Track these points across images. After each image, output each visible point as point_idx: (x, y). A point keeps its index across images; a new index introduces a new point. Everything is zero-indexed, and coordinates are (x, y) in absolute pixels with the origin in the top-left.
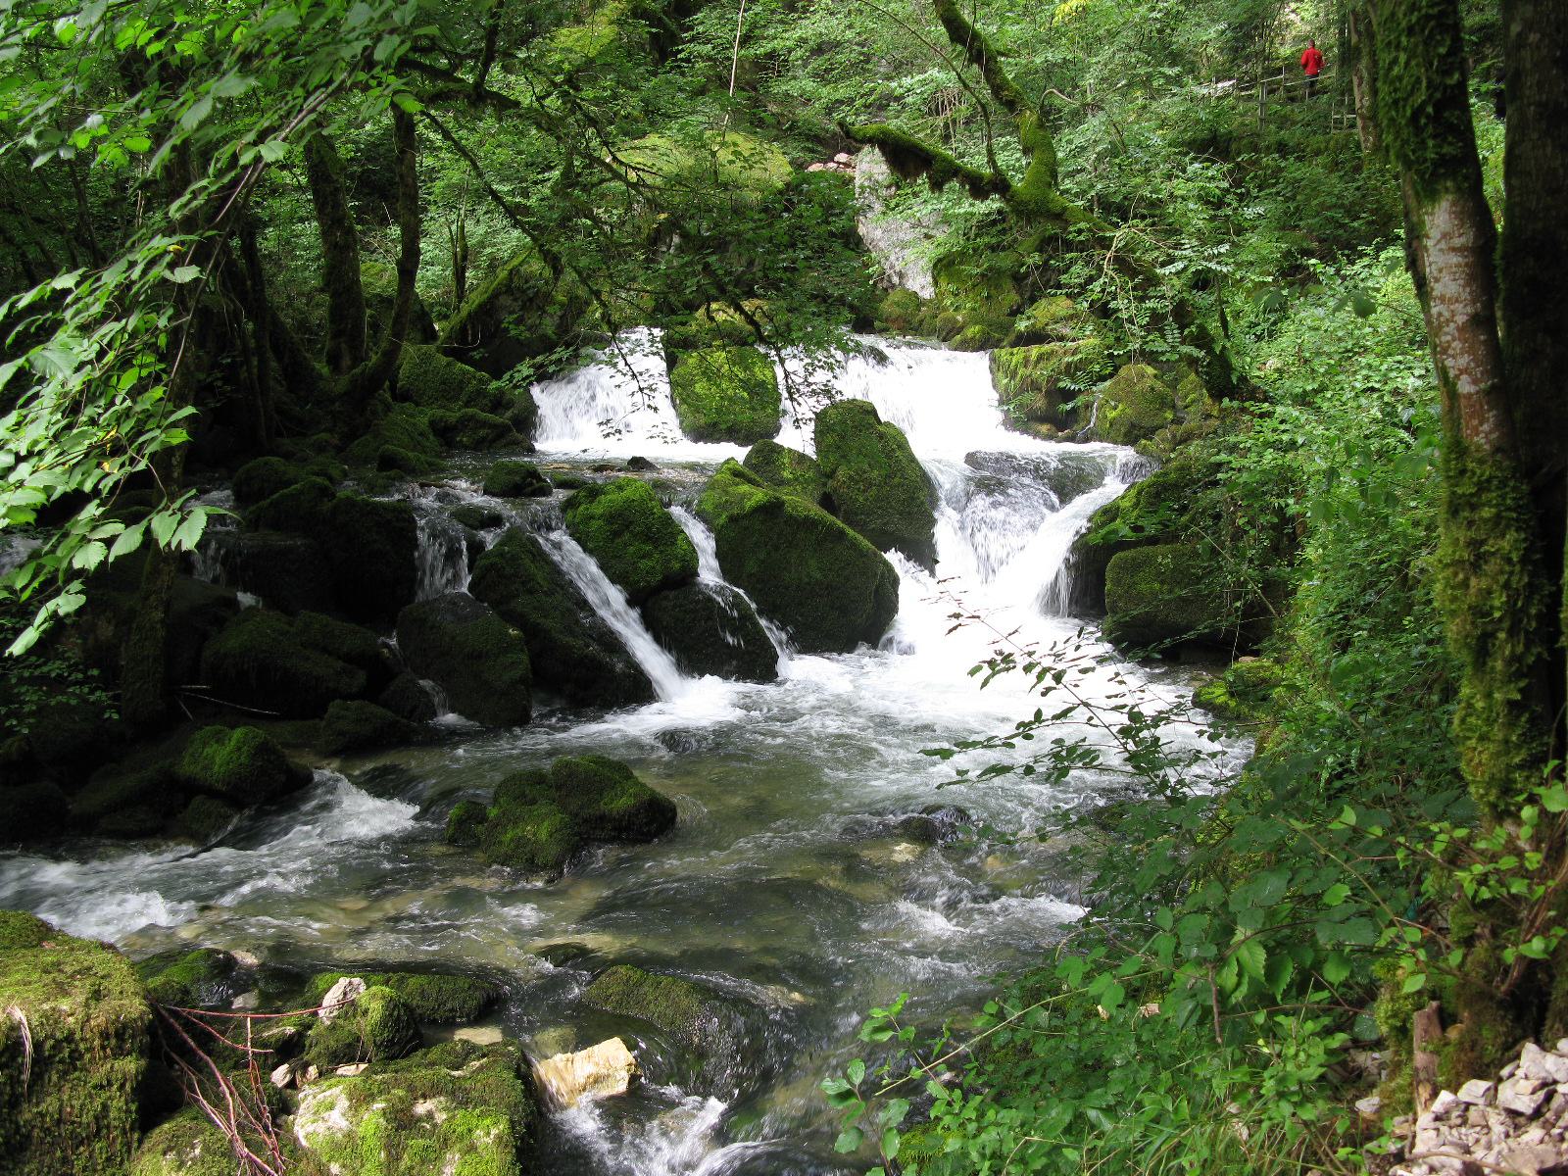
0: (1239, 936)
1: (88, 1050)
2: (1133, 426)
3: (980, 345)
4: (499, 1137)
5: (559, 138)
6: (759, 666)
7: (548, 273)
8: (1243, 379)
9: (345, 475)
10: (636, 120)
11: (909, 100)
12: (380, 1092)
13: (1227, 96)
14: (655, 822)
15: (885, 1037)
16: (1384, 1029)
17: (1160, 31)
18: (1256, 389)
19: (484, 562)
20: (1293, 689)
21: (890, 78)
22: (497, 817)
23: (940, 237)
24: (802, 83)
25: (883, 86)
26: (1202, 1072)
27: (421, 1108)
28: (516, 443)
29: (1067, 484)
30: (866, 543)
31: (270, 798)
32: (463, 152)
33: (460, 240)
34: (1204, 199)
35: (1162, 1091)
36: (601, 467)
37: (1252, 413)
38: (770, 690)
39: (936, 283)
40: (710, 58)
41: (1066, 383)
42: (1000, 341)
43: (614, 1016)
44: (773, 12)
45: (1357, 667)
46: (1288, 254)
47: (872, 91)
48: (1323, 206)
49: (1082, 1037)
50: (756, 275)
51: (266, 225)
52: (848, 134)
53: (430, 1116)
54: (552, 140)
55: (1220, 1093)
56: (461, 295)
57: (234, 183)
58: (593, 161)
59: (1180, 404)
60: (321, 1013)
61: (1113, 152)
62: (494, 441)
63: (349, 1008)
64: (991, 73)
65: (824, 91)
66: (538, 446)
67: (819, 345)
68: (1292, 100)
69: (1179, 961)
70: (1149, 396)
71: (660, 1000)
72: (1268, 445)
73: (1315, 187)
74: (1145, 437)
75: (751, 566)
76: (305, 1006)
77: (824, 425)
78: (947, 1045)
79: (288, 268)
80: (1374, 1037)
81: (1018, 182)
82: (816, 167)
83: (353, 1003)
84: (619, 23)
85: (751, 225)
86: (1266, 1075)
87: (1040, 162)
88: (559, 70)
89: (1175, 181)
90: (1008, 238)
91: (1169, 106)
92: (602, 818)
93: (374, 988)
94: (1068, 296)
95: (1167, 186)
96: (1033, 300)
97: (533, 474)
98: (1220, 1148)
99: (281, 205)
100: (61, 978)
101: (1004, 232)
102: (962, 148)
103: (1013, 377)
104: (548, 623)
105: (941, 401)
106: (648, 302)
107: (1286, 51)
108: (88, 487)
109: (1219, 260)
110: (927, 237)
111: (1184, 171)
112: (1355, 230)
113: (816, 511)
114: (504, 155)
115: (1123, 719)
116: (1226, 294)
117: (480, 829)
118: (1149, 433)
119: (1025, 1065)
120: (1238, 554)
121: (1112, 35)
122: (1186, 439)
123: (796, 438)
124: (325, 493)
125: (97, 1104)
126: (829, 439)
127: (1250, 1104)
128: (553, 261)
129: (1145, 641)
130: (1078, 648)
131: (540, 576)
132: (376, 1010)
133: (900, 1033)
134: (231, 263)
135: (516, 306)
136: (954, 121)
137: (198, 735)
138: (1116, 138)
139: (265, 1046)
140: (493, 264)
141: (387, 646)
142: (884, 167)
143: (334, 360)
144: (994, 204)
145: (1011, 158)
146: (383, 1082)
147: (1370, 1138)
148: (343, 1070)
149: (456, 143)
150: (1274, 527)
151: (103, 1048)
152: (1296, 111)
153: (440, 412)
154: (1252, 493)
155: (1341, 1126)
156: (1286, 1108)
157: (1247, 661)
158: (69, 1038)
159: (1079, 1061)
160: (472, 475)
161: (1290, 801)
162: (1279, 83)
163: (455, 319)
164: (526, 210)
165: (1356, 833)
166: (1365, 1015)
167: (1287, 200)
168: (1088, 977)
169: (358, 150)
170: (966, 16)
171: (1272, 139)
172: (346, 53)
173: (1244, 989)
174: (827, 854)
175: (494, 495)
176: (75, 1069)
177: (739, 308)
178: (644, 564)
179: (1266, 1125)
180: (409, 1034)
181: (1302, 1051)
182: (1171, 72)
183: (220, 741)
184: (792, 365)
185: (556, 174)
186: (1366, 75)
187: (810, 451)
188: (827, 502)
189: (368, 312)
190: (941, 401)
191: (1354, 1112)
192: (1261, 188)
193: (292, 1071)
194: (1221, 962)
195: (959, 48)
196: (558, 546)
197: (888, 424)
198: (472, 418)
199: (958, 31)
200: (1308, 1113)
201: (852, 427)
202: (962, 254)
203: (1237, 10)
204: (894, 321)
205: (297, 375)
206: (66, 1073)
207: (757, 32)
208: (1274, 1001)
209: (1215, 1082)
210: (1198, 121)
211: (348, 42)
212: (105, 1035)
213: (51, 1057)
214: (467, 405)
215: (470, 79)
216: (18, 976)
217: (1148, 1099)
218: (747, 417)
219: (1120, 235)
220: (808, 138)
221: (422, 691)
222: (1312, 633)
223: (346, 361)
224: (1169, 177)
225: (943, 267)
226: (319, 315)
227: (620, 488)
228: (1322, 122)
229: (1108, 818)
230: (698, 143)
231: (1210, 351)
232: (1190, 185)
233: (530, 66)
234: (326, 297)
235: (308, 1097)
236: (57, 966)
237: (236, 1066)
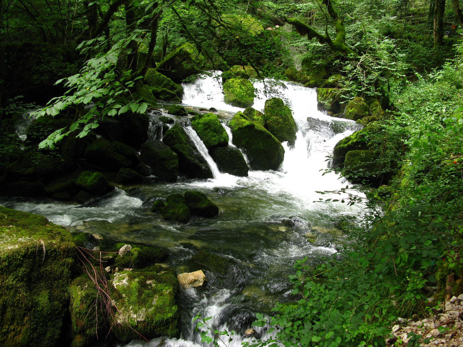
0: (401, 250)
1: (59, 255)
4: (170, 293)
8: (392, 104)
19: (168, 133)
28: (177, 100)
29: (336, 129)
30: (277, 140)
31: (101, 193)
36: (202, 110)
37: (394, 114)
38: (244, 179)
42: (320, 85)
48: (420, 57)
53: (150, 284)
59: (371, 110)
62: (170, 98)
63: (128, 253)
74: (359, 118)
97: (183, 109)
100: (52, 234)
104: (184, 152)
105: (302, 102)
108: (111, 94)
118: (361, 117)
125: (61, 269)
131: (183, 139)
132: (136, 254)
137: (83, 173)
145: (332, 31)
148: (125, 269)
151: (64, 255)
153: (156, 88)
158: (55, 250)
160: (165, 107)
162: (410, 18)
163: (162, 62)
167: (410, 53)
171: (407, 35)
175: (171, 114)
176: (56, 259)
183: (89, 176)
186: (438, 19)
188: (266, 126)
193: (111, 268)
194: (396, 257)
198: (165, 91)
201: (277, 106)
206: (53, 260)
212: (64, 251)
213: (50, 255)
214: (163, 87)
216: (41, 232)
218: (243, 101)
219: (362, 58)
221: (147, 168)
225: (306, 62)
227: (208, 116)
236: (51, 231)
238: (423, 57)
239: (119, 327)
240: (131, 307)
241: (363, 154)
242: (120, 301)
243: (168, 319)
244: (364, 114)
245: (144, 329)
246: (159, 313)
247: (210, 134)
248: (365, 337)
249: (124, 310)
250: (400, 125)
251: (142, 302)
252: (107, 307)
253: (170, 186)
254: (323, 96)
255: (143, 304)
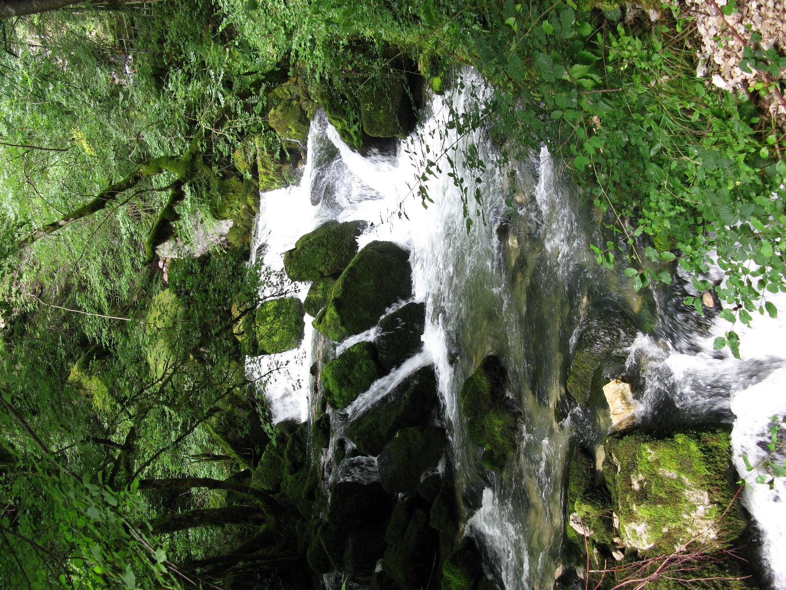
0: (566, 77)
2: (300, 121)
3: (257, 197)
4: (652, 448)
5: (150, 408)
6: (416, 314)
7: (217, 414)
8: (278, 65)
9: (317, 517)
10: (140, 368)
11: (133, 230)
12: (628, 507)
13: (133, 68)
14: (494, 367)
15: (612, 256)
16: (616, 6)
17: (100, 102)
18: (283, 59)
19: (362, 449)
20: (437, 44)
21: (122, 239)
22: (490, 445)
23: (202, 216)
24: (123, 284)
25: (125, 243)
26: (635, 98)
27: (636, 486)
29: (330, 154)
32: (156, 456)
33: (199, 458)
34: (187, 82)
35: (642, 118)
36: (315, 389)
37: (296, 61)
38: (429, 309)
39: (225, 218)
40: (109, 330)
41: (277, 155)
42: (255, 187)
43: (592, 390)
44: (86, 297)
45: (427, 12)
46: (215, 40)
47: (128, 249)
49: (613, 157)
50: (220, 309)
51: (190, 555)
52: (150, 262)
53: (640, 482)
54: (151, 411)
55: (645, 89)
56: (227, 457)
57: (176, 575)
58: (162, 391)
59: (289, 97)
60: (587, 535)
61: (161, 127)
63: (585, 521)
64: (120, 188)
65: (127, 272)
66: (303, 421)
67: (258, 279)
68: (136, 35)
69: (579, 108)
70: (285, 112)
71: (584, 366)
72: (311, 54)
73: (180, 26)
75: (366, 315)
76: (583, 543)
77: (297, 277)
78: (616, 227)
79: (211, 544)
80: (619, 11)
81: (176, 176)
82: (166, 277)
83: (583, 519)
84: (90, 374)
85: (196, 311)
86: (639, 66)
87: (166, 164)
88: (115, 406)
89: (178, 97)
90: (204, 181)
91: (138, 97)
92: (492, 393)
93: (576, 509)
94: (234, 152)
95: (180, 101)
96: (235, 170)
97: (318, 423)
98: (673, 90)
99: (180, 546)
101: (200, 184)
102: (158, 204)
103: (274, 181)
104: (393, 418)
105: (285, 218)
106: (234, 364)
107: (111, 38)
109: (217, 75)
110: (202, 222)
111: (172, 92)
112: (203, 6)
113: (339, 282)
114: (157, 435)
115: (453, 132)
116: (235, 72)
117: (496, 453)
118: (304, 113)
119: (624, 185)
120: (367, 69)
121: (102, 126)
122: (307, 94)
123: (302, 291)
124: (325, 528)
126: (304, 274)
127: (651, 74)
128: (211, 412)
129: (410, 117)
130: (415, 153)
132: (586, 508)
133: (610, 249)
134: (209, 573)
135: (233, 430)
136: (144, 207)
138: (155, 126)
139: (603, 564)
140: (212, 441)
141: (403, 498)
142: (166, 243)
143: (259, 522)
144: (186, 188)
145: (163, 180)
146: (623, 505)
147: (671, 15)
149: (151, 459)
150: (353, 51)
152: (142, 34)
153: (286, 469)
154: (336, 60)
155: (666, 30)
156: (655, 57)
157: (421, 67)
159: (625, 158)
160: (317, 457)
161: (499, 47)
163: (239, 461)
164: (185, 424)
165: (518, 16)
166: (608, 16)
168: (585, 154)
169: (153, 508)
170: (90, 200)
171: (156, 47)
172: (113, 520)
173: (595, 76)
174: (512, 280)
177: (238, 319)
178: (364, 368)
179: (664, 67)
180: (599, 492)
181: (627, 47)
182: (121, 97)
184: (267, 293)
185: (166, 408)
187: (309, 286)
188: (335, 276)
189: (234, 504)
190: (285, 218)
191: (657, 22)
192: (181, 53)
193: (616, 550)
194: (580, 87)
195: (107, 204)
196: (355, 411)
197: (296, 245)
198: (289, 453)
199: (98, 204)
200: (658, 46)
201: (298, 262)
202: (211, 205)
203: (90, 62)
204: (244, 240)
205: (266, 540)
207: (96, 305)
208: (601, 61)
209: (640, 92)
210: (147, 84)
211: (108, 518)
214: (282, 455)
215: (119, 451)
217: (646, 125)
218: (290, 315)
219: (204, 125)
220: (151, 280)
221: (426, 480)
222: (408, 34)
223: (259, 516)
224: (175, 99)
225: (217, 214)
226: (236, 529)
227: (326, 379)
228: (148, 20)
229: (497, 140)
230: (154, 337)
231: (264, 81)
232: (180, 89)
233: (113, 421)
234: (226, 525)
235: (629, 542)
237: (613, 578)
238: (191, 16)
239: (724, 534)
240: (686, 516)
241: (367, 107)
242: (675, 536)
243: (701, 450)
244: (298, 109)
245: (723, 490)
246: (691, 467)
247: (357, 375)
248: (753, 150)
249: (692, 528)
250: (312, 49)
251: (673, 497)
252: (688, 557)
253: (454, 439)
254: (273, 180)
255: (678, 494)
